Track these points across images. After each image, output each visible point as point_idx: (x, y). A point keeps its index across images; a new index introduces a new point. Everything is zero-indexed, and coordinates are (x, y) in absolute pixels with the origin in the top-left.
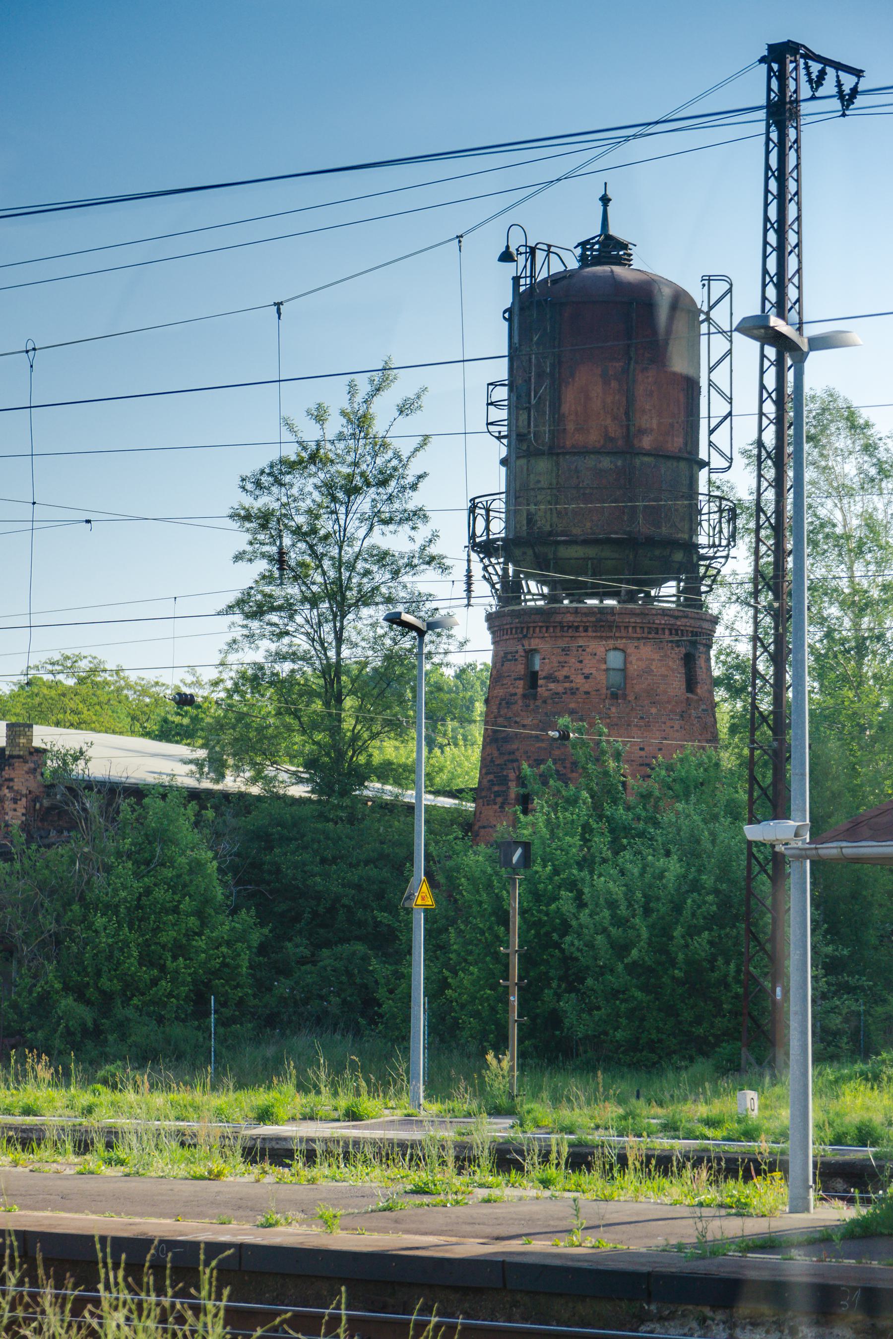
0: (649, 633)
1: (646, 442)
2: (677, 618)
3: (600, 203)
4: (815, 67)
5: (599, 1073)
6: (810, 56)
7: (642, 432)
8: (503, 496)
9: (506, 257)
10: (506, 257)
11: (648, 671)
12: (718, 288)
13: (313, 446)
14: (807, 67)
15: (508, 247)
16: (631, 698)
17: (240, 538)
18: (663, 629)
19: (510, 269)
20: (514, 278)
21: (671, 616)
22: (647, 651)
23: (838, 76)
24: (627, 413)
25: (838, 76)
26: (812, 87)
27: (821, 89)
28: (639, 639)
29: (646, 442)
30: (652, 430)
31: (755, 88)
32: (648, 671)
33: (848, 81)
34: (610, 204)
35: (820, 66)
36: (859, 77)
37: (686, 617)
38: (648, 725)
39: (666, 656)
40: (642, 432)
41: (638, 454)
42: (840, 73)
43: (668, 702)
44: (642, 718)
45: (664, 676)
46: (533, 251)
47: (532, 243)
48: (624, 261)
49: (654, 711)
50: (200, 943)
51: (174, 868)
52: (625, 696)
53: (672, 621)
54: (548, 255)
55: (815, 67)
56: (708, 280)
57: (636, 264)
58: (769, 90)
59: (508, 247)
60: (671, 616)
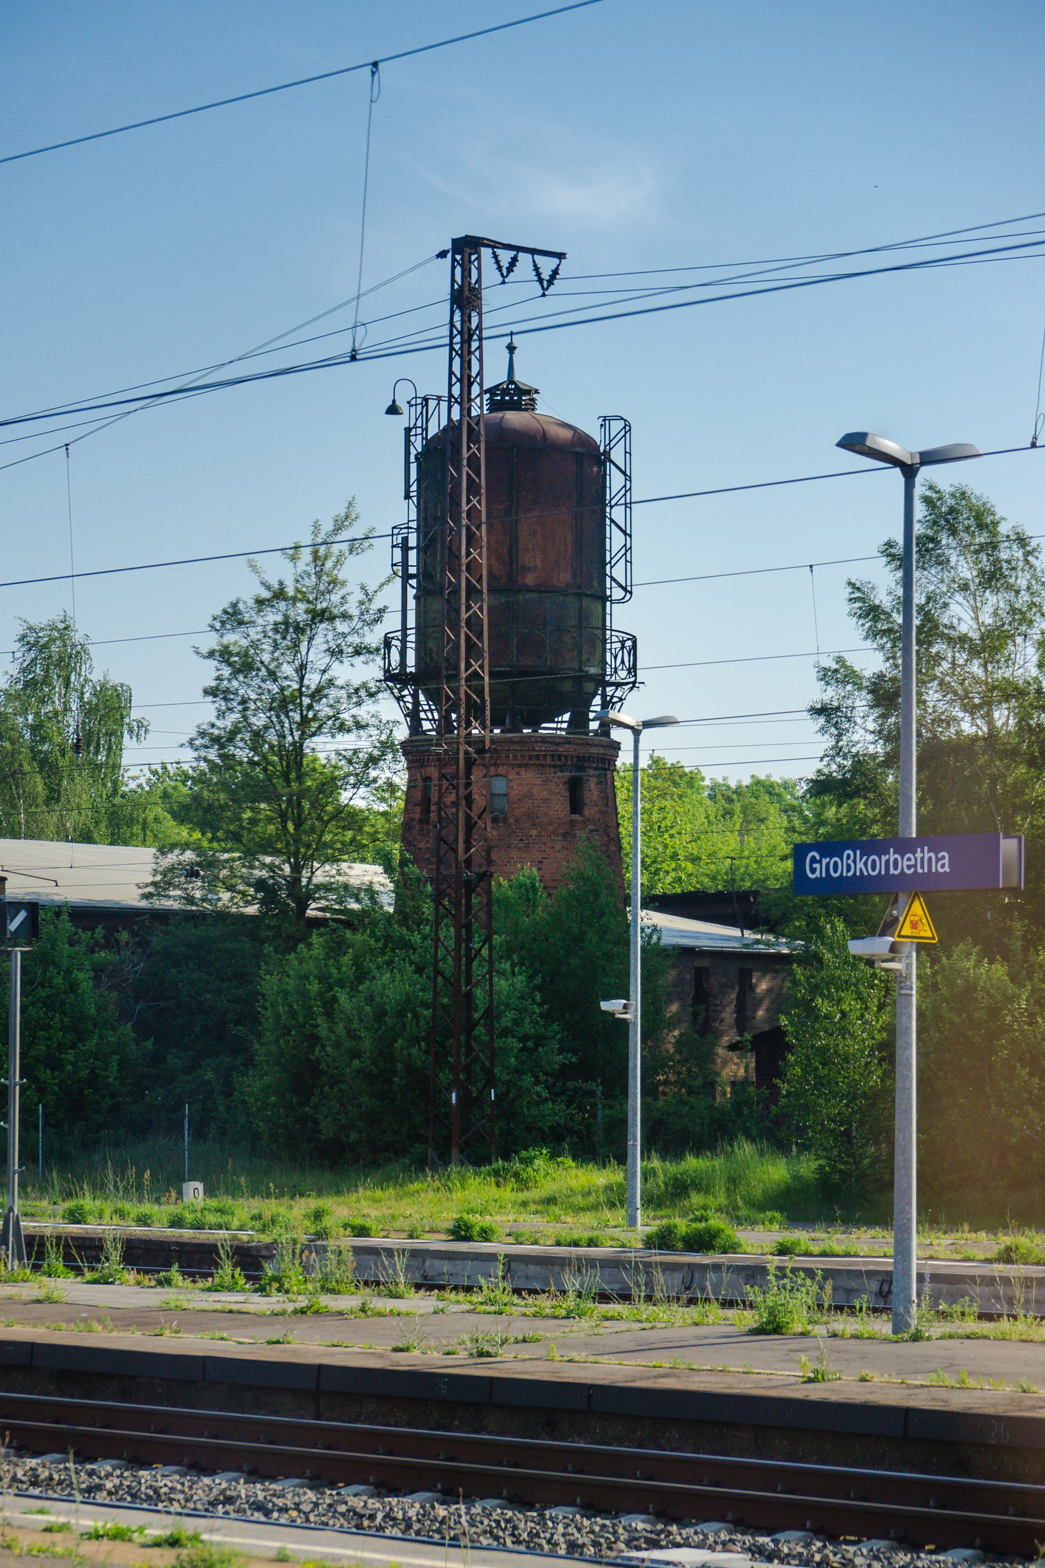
0: (530, 759)
1: (530, 579)
2: (558, 744)
3: (507, 351)
4: (505, 256)
5: (55, 1173)
6: (494, 245)
7: (526, 569)
8: (399, 633)
9: (393, 410)
10: (393, 410)
11: (529, 795)
12: (617, 426)
13: (276, 586)
14: (495, 256)
15: (394, 401)
16: (512, 821)
17: (209, 672)
18: (545, 756)
19: (401, 422)
20: (406, 429)
21: (552, 743)
22: (529, 776)
23: (534, 261)
24: (510, 552)
25: (534, 261)
26: (502, 275)
27: (512, 274)
28: (520, 766)
29: (530, 579)
30: (535, 568)
31: (440, 279)
32: (529, 795)
33: (547, 265)
34: (516, 352)
35: (513, 253)
36: (560, 259)
37: (570, 743)
38: (527, 846)
39: (548, 780)
40: (526, 569)
41: (520, 591)
42: (536, 256)
43: (550, 824)
44: (521, 840)
45: (545, 800)
46: (426, 400)
47: (421, 394)
48: (532, 405)
49: (534, 832)
50: (70, 1056)
51: (51, 987)
52: (505, 820)
53: (553, 748)
54: (438, 404)
55: (505, 256)
56: (606, 420)
57: (541, 409)
58: (453, 281)
59: (394, 401)
60: (552, 743)
